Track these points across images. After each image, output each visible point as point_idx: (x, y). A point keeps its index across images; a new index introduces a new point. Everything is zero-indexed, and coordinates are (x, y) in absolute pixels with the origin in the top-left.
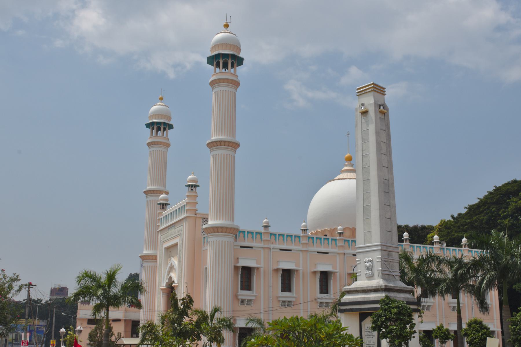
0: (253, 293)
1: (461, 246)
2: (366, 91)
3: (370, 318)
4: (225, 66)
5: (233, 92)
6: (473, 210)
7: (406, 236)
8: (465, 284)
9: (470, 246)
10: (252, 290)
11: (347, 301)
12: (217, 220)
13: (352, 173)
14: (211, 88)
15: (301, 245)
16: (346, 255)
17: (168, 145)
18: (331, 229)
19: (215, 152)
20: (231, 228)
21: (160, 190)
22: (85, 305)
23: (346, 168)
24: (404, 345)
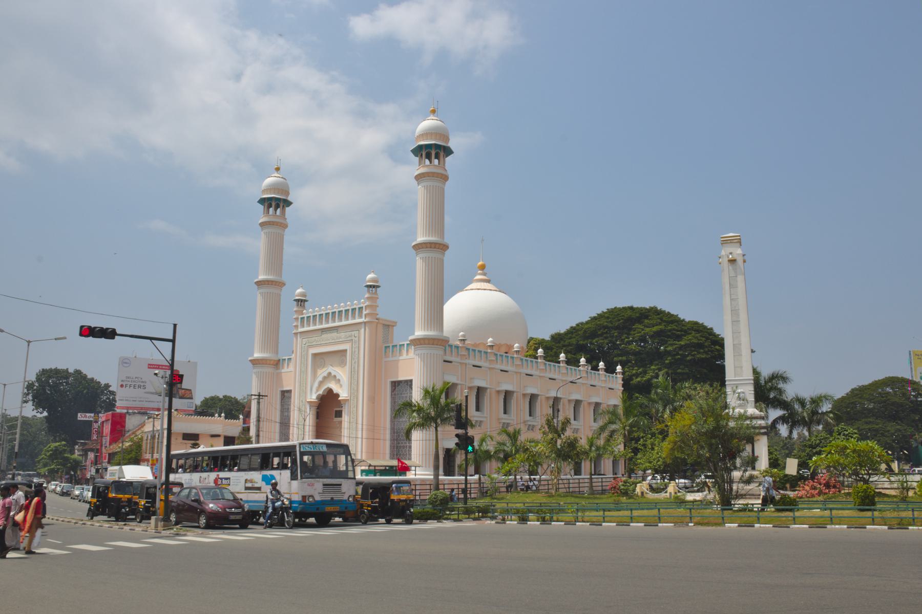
2: (732, 241)
4: (428, 156)
6: (573, 331)
7: (583, 361)
10: (480, 411)
12: (431, 330)
13: (485, 283)
14: (417, 183)
15: (514, 366)
17: (285, 226)
19: (264, 231)
20: (438, 340)
21: (276, 280)
23: (478, 277)
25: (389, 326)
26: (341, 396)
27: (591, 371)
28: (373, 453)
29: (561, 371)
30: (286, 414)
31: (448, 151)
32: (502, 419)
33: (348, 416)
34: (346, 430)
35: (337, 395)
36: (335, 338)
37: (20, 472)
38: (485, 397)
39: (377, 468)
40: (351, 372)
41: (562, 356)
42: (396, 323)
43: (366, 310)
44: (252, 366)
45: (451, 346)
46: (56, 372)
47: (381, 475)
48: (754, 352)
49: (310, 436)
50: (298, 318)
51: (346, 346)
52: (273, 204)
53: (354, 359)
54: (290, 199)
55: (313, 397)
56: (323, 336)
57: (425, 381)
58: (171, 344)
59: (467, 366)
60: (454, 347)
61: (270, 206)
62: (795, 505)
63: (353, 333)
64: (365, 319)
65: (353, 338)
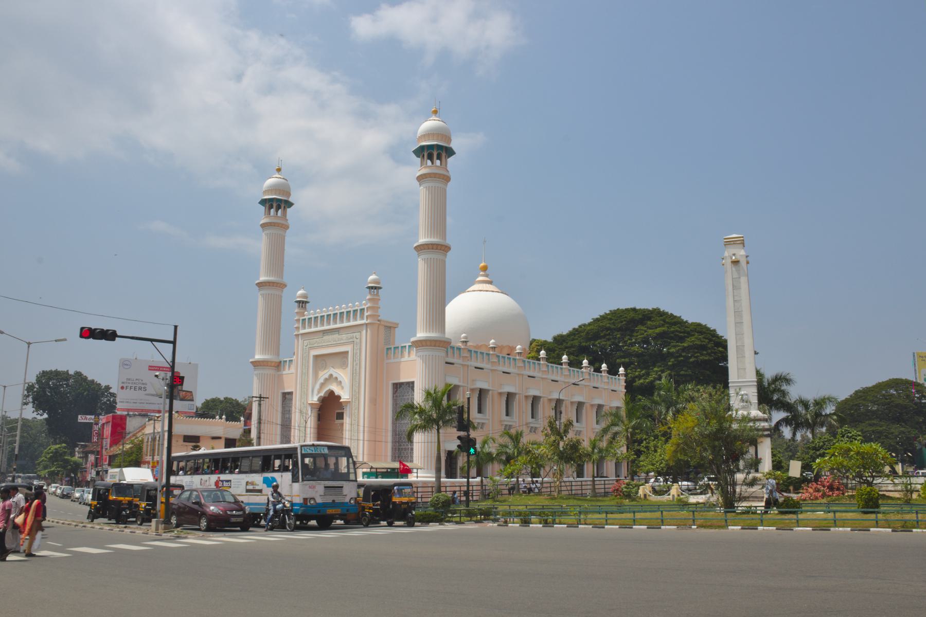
2: (735, 242)
3: (472, 470)
4: (430, 157)
6: (575, 333)
7: (585, 363)
8: (563, 435)
10: (483, 413)
12: (433, 332)
13: (487, 285)
14: (419, 183)
15: (517, 368)
17: (286, 227)
20: (440, 341)
21: (277, 282)
23: (480, 278)
24: (708, 482)
25: (390, 327)
26: (342, 398)
27: (594, 373)
28: (375, 455)
29: (563, 373)
30: (287, 416)
33: (349, 418)
34: (347, 432)
35: (339, 397)
36: (337, 340)
37: (20, 475)
38: (487, 399)
39: (378, 470)
40: (353, 374)
41: (565, 358)
42: (398, 324)
43: (367, 312)
44: (253, 367)
45: (453, 348)
46: (56, 374)
47: (382, 478)
48: (758, 353)
49: (312, 438)
50: (299, 320)
51: (348, 348)
52: (275, 205)
53: (355, 361)
54: (291, 200)
55: (315, 399)
56: (325, 338)
57: (427, 383)
58: (171, 345)
59: (469, 368)
60: (455, 349)
61: (271, 207)
62: (799, 508)
63: (354, 334)
64: (367, 320)
65: (355, 340)
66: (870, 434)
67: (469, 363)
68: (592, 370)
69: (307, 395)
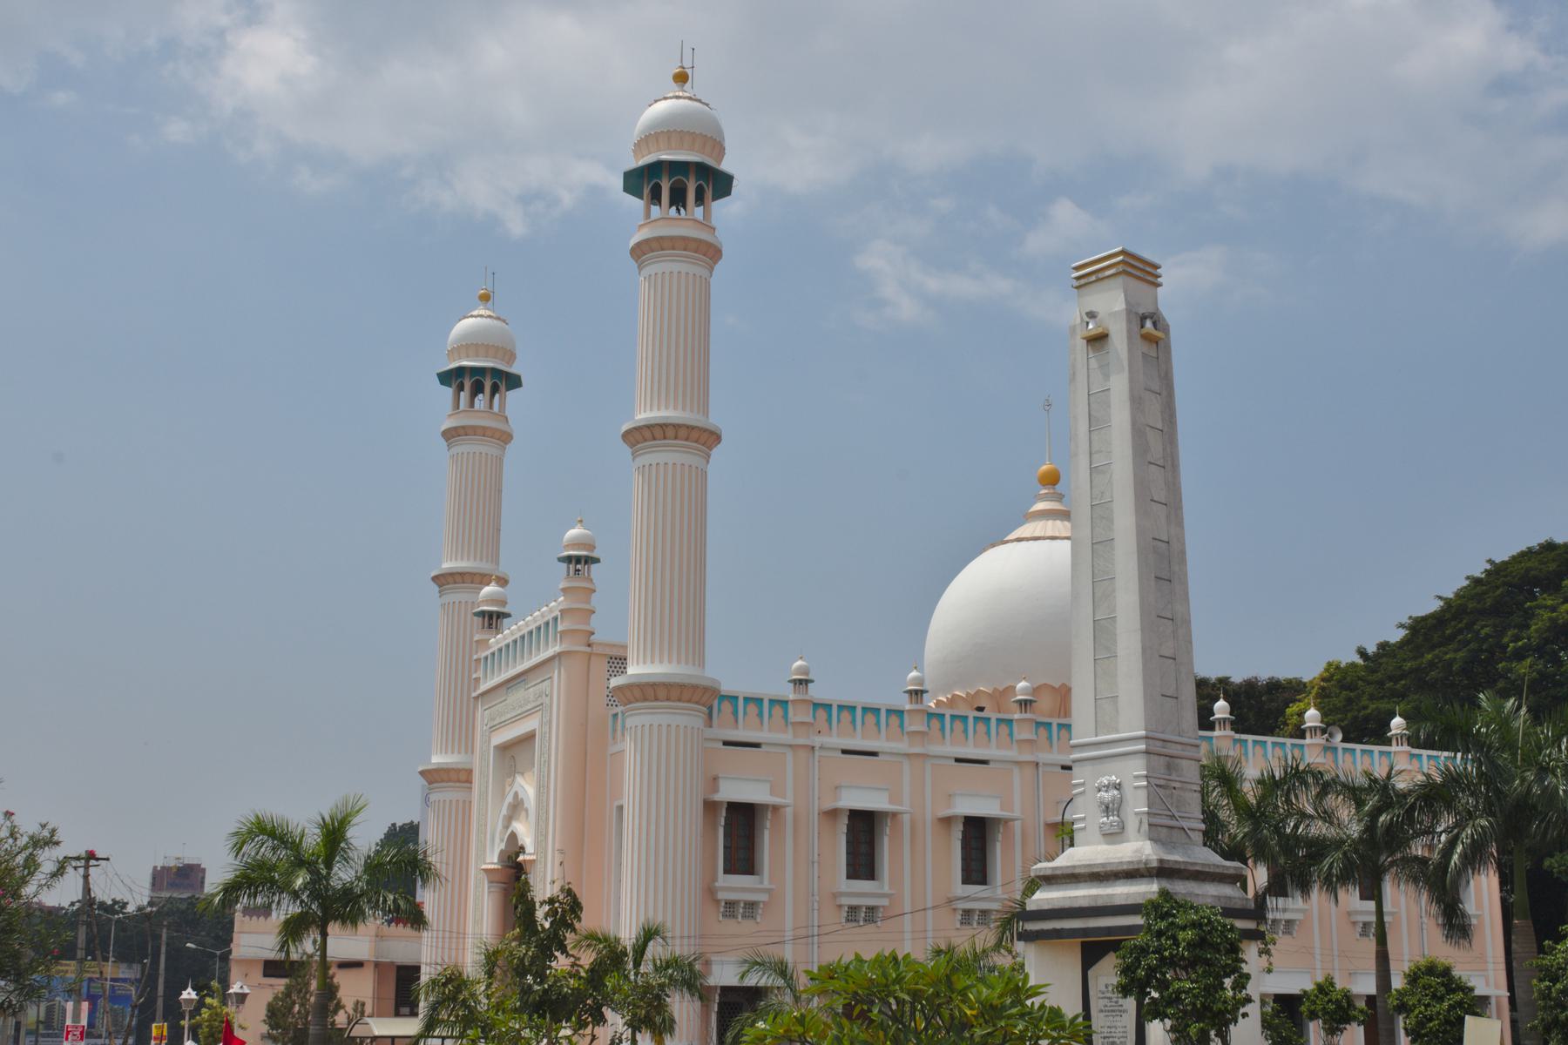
0: (762, 883)
1: (1388, 742)
2: (1101, 275)
4: (678, 199)
5: (701, 277)
6: (1423, 631)
7: (1222, 710)
9: (1413, 741)
10: (758, 875)
11: (1046, 907)
12: (652, 662)
13: (1058, 522)
14: (636, 265)
15: (906, 736)
16: (1040, 769)
17: (505, 438)
18: (995, 690)
19: (647, 459)
20: (695, 687)
21: (482, 571)
22: (254, 918)
23: (1041, 506)
31: (720, 184)
32: (1357, 913)
60: (883, 714)
66: (20, 944)
67: (817, 741)
68: (1339, 737)
69: (485, 851)
